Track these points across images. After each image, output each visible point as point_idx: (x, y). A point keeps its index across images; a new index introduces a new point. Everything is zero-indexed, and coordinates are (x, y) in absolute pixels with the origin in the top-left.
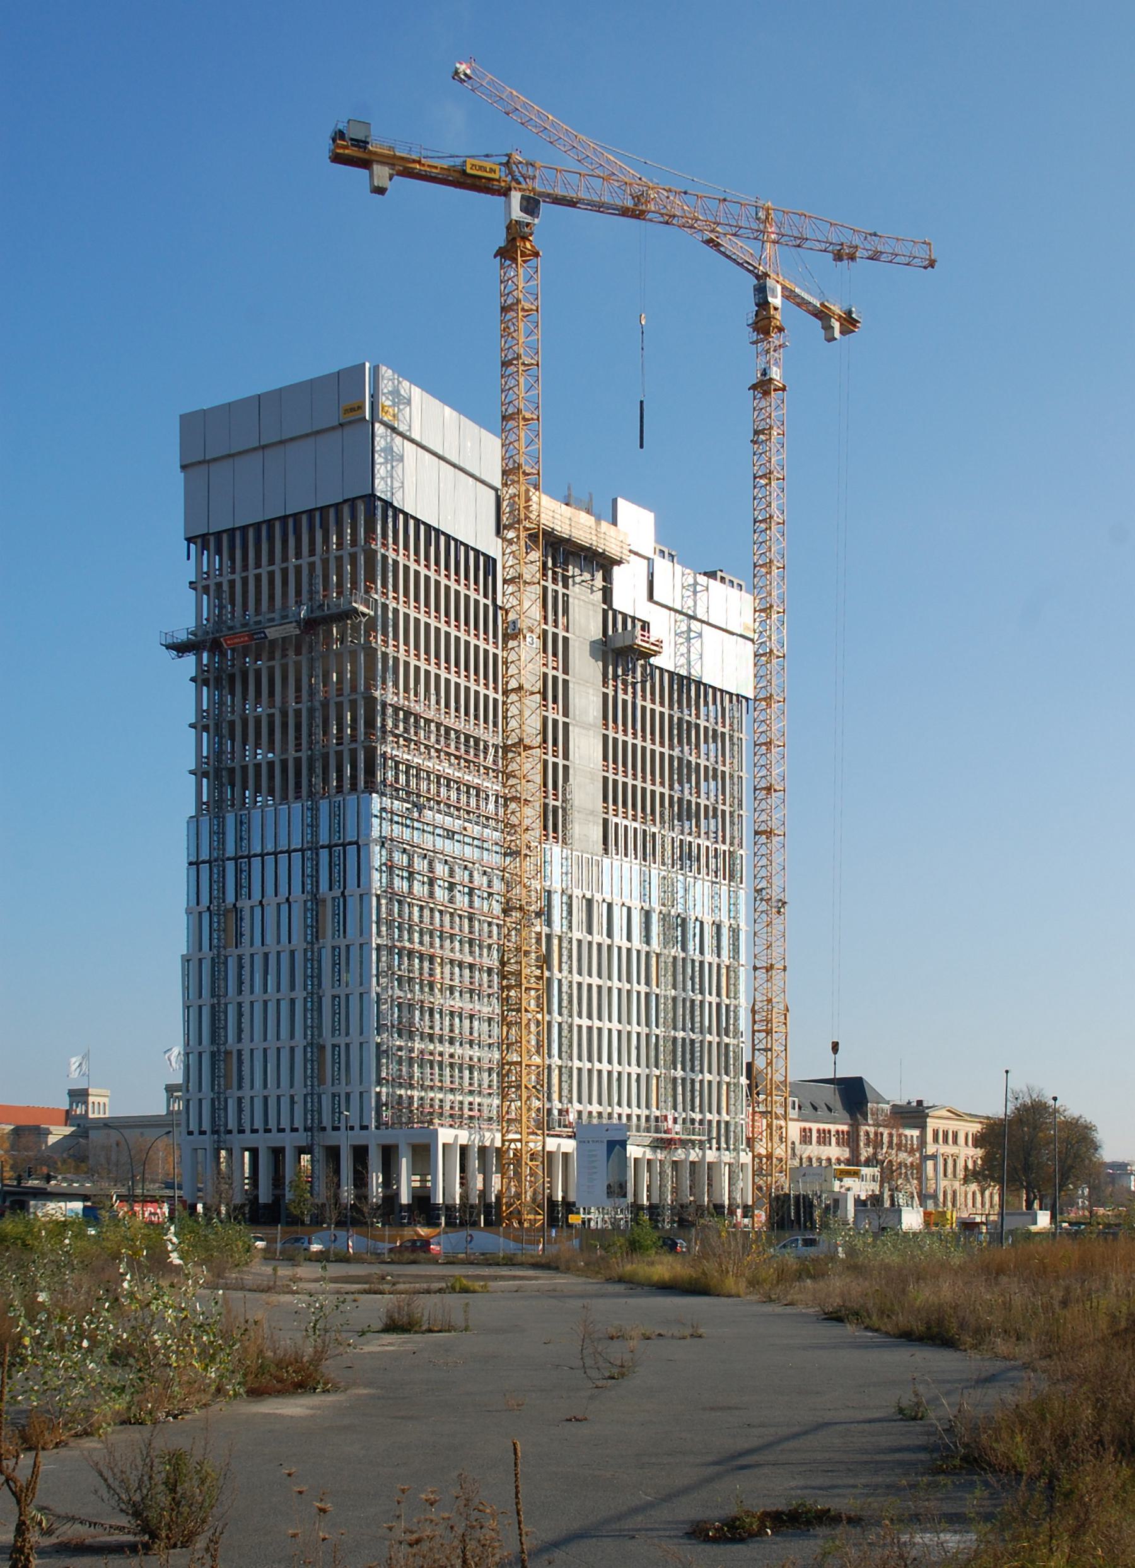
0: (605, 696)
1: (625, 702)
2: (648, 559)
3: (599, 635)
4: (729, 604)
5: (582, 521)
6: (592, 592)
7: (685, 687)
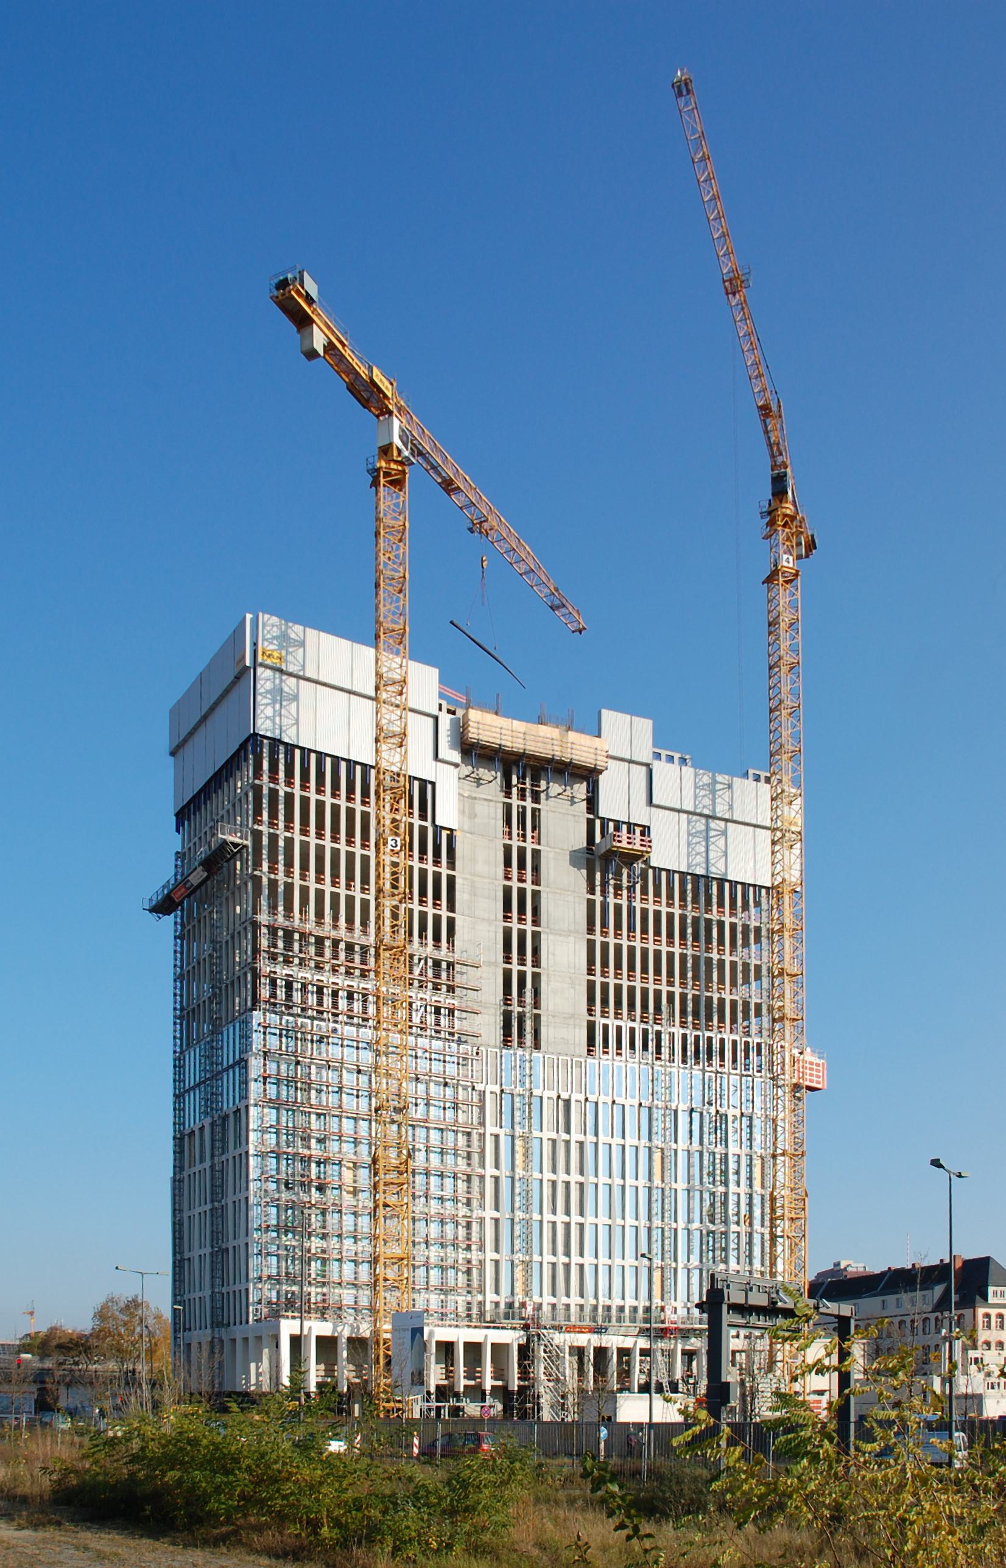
0: (591, 904)
1: (618, 908)
2: (648, 765)
3: (583, 843)
4: (751, 798)
5: (542, 734)
6: (573, 803)
7: (701, 887)
